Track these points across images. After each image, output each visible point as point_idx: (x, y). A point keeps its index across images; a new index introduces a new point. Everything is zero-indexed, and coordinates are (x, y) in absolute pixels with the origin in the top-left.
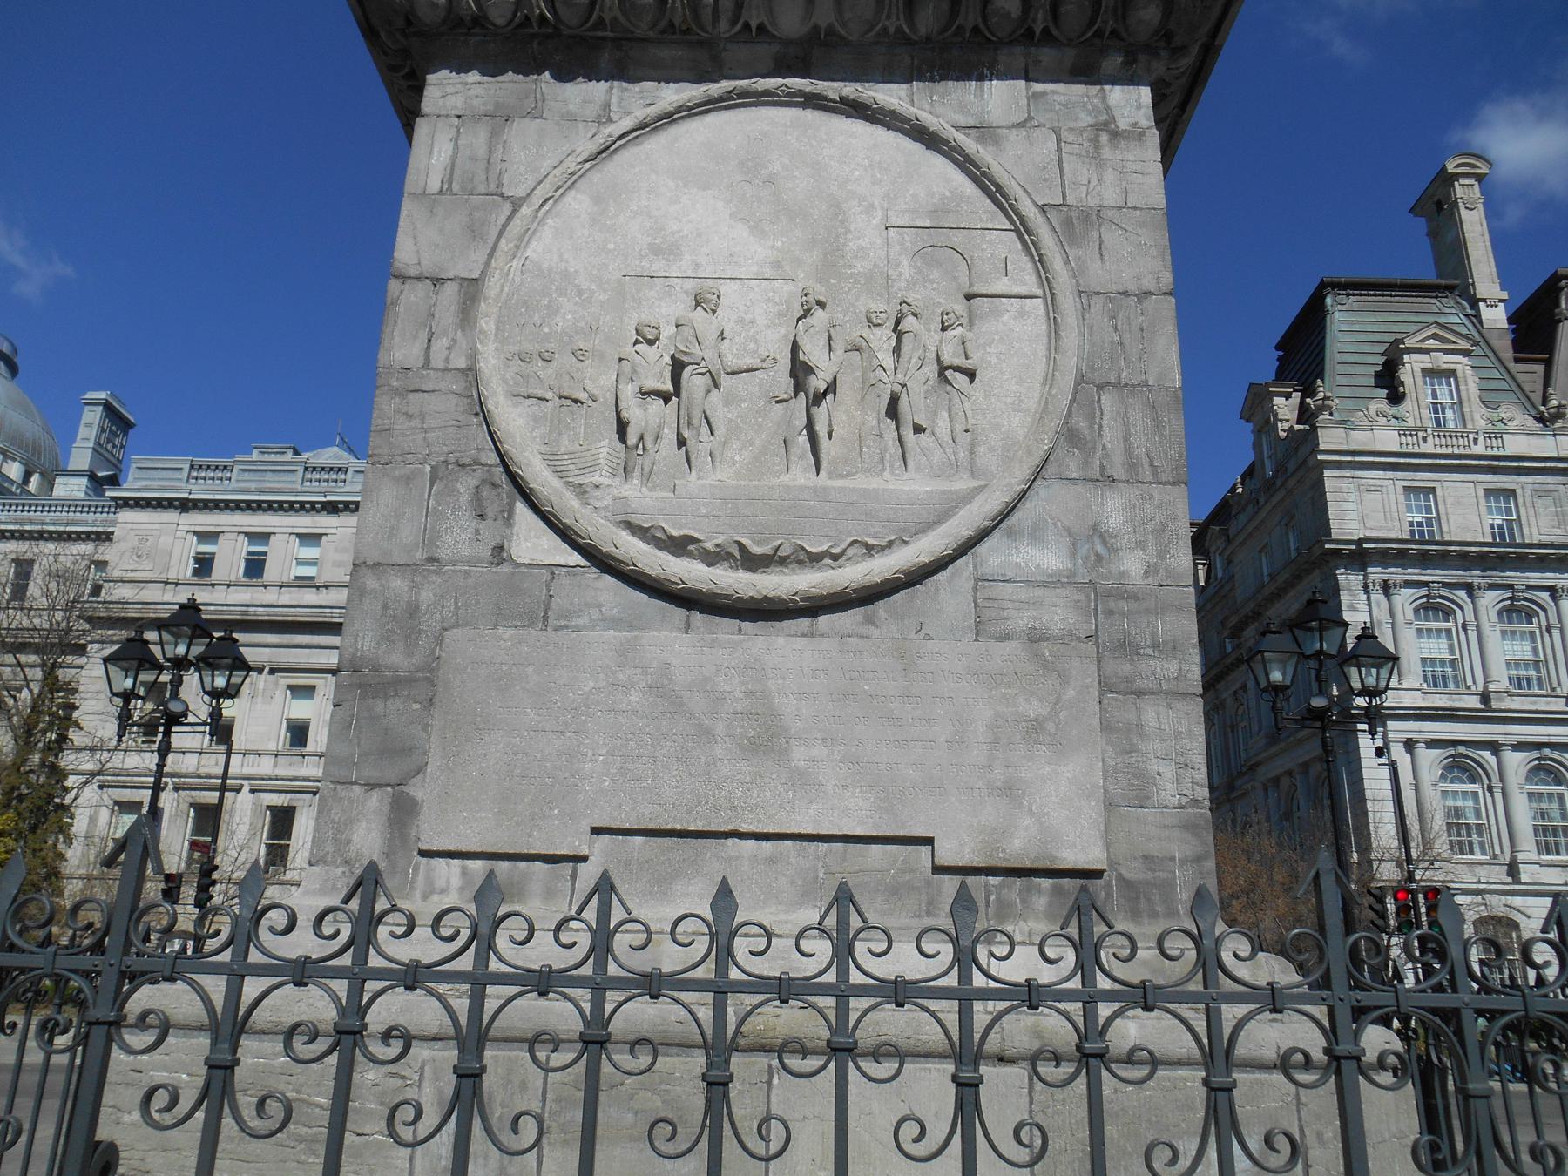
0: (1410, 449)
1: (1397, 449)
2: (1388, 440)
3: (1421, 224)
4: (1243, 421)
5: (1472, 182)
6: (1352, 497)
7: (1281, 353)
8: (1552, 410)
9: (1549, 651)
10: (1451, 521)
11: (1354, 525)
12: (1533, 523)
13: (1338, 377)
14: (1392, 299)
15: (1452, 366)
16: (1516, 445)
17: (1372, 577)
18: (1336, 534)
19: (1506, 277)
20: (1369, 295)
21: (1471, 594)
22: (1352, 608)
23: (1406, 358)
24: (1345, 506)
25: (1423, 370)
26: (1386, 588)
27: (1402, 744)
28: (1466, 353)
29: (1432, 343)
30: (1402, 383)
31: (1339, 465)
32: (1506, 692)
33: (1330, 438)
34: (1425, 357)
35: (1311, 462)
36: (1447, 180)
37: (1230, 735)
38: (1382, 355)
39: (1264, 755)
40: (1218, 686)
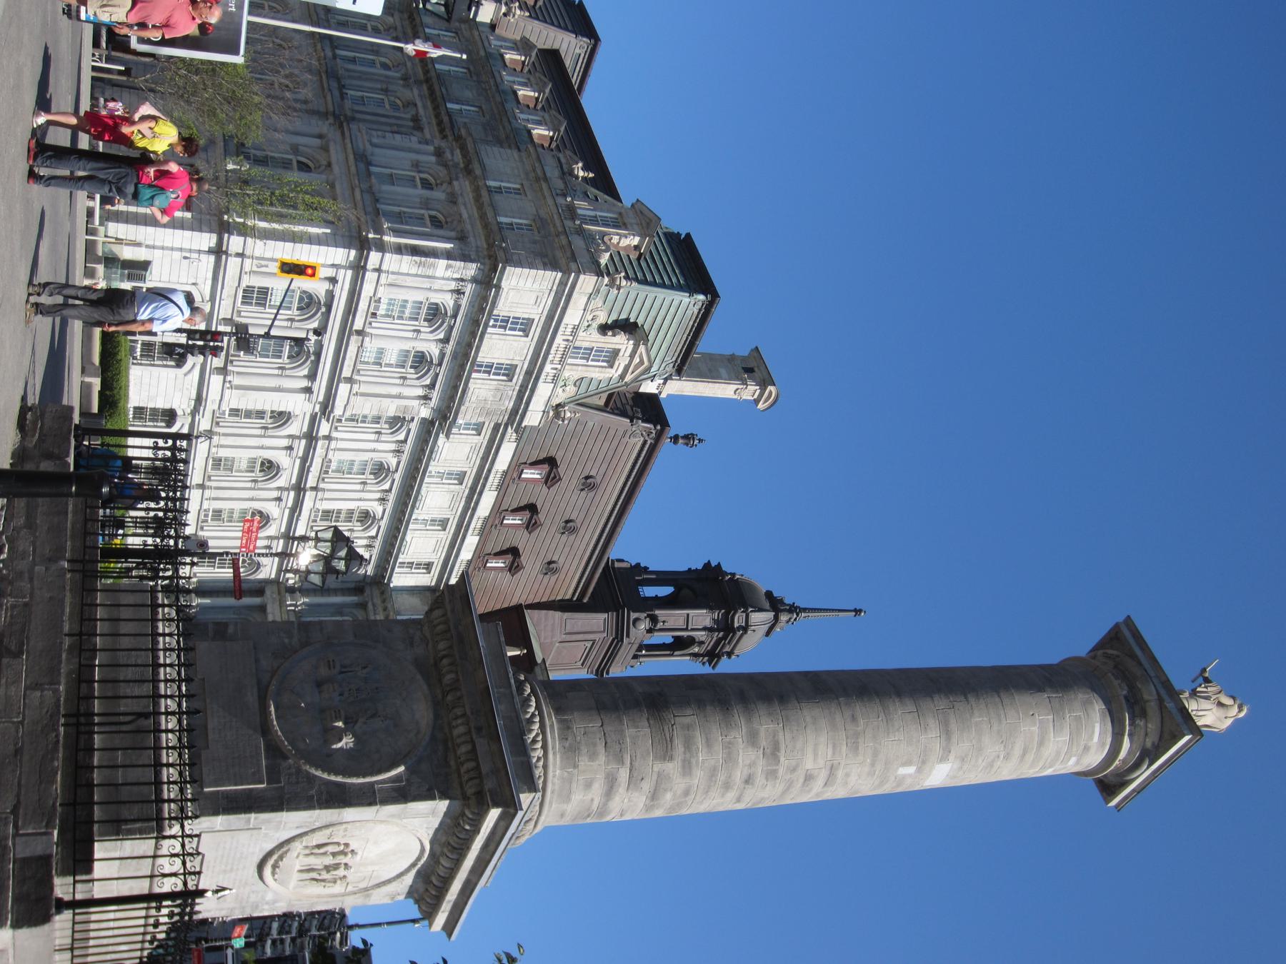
0: (561, 329)
1: (566, 320)
2: (573, 316)
3: (744, 351)
4: (634, 201)
5: (756, 397)
6: (536, 286)
7: (683, 237)
8: (563, 414)
9: (387, 374)
10: (499, 341)
11: (514, 282)
12: (483, 387)
13: (636, 293)
14: (685, 335)
15: (615, 367)
16: (543, 392)
17: (470, 286)
18: (510, 270)
19: (676, 399)
20: (695, 322)
21: (441, 341)
22: (448, 267)
23: (631, 342)
24: (530, 280)
25: (619, 350)
26: (459, 292)
27: (334, 275)
28: (622, 377)
29: (637, 360)
30: (614, 335)
31: (563, 284)
32: (362, 346)
33: (587, 282)
34: (628, 353)
35: (573, 266)
36: (764, 382)
37: (379, 86)
38: (642, 326)
39: (349, 145)
40: (425, 87)
